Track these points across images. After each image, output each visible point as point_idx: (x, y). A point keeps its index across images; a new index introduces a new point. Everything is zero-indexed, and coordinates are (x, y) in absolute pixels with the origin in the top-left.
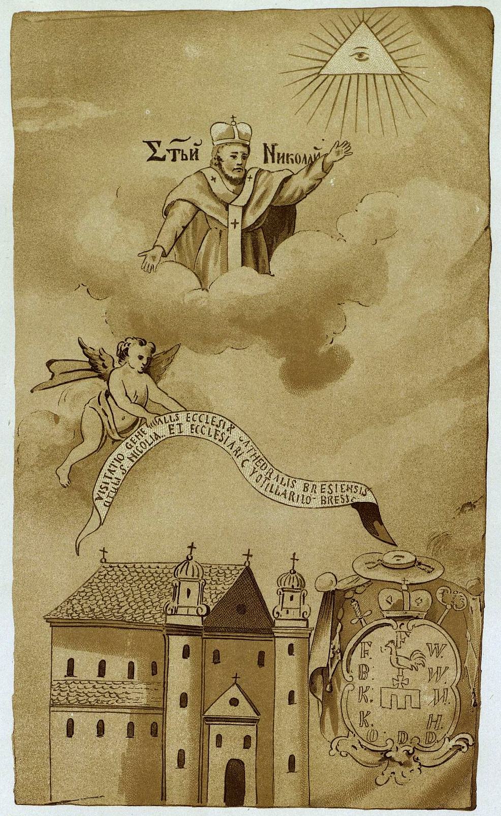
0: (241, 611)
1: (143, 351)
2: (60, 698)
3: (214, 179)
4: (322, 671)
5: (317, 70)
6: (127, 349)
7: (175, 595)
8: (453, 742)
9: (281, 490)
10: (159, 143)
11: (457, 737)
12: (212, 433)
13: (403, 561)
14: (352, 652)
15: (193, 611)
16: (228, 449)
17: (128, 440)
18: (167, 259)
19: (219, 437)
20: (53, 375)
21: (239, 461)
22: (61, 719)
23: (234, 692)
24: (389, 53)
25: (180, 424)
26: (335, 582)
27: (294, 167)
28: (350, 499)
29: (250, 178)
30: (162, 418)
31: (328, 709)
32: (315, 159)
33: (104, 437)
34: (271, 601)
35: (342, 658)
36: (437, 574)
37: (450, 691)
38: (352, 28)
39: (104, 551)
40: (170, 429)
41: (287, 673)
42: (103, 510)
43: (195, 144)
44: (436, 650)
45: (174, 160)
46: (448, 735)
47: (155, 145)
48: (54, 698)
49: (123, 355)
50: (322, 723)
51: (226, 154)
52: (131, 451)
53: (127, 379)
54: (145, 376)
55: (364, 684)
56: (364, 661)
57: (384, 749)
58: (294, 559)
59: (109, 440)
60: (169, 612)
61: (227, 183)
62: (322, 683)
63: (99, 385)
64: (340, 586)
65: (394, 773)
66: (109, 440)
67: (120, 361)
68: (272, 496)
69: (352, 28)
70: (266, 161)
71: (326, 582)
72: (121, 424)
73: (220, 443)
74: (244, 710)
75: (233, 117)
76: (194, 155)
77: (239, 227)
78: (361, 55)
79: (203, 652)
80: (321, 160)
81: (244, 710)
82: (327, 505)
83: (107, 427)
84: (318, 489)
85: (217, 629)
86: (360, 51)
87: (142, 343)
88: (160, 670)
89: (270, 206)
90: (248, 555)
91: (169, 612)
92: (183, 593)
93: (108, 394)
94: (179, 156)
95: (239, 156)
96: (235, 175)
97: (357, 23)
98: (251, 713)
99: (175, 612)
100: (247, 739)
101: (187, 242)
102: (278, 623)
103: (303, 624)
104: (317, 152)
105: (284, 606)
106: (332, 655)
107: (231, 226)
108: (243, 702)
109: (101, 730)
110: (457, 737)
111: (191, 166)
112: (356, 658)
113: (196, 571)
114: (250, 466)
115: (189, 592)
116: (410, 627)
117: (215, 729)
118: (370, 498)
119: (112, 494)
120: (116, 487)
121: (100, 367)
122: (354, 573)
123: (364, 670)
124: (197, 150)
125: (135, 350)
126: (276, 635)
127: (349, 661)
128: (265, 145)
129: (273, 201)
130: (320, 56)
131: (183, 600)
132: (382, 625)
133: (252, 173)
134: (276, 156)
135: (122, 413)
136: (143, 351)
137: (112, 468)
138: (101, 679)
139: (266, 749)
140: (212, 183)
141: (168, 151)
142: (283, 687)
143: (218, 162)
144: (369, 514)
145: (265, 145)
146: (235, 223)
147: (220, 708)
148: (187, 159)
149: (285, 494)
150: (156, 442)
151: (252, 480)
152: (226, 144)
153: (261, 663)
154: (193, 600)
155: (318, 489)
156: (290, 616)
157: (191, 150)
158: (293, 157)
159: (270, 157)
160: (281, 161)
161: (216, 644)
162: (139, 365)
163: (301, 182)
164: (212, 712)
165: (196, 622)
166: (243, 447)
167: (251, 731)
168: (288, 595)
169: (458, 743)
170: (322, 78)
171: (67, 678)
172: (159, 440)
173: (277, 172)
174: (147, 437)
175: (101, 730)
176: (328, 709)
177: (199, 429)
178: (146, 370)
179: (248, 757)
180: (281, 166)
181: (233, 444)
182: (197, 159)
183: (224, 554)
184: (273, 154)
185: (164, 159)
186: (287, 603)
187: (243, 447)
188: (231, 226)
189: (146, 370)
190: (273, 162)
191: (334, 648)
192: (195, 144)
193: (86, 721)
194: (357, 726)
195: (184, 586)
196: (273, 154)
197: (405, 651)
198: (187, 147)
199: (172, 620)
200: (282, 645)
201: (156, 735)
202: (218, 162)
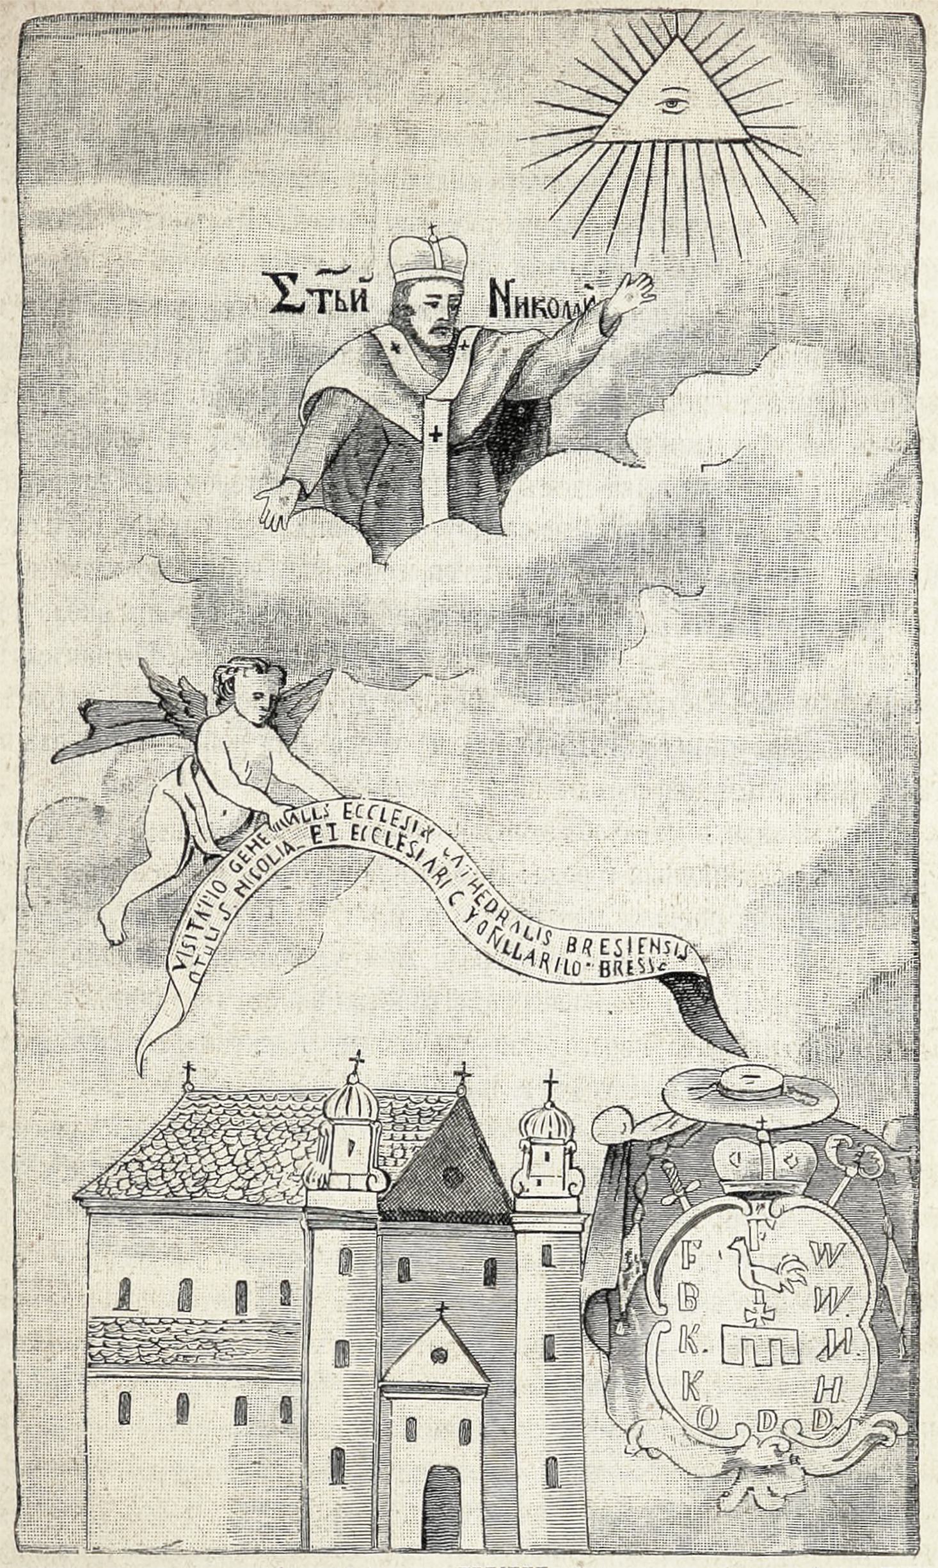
0: (445, 1182)
1: (268, 684)
3: (396, 348)
4: (607, 1295)
5: (587, 135)
6: (232, 680)
7: (326, 1153)
8: (866, 1429)
9: (524, 951)
10: (293, 277)
11: (874, 1419)
12: (394, 841)
13: (757, 1085)
14: (664, 1260)
15: (359, 1182)
16: (423, 872)
17: (234, 856)
18: (309, 502)
19: (406, 849)
20: (93, 728)
21: (444, 894)
23: (440, 1337)
24: (644, 73)
25: (332, 825)
26: (629, 1127)
27: (550, 325)
28: (656, 965)
29: (464, 346)
30: (298, 813)
32: (587, 308)
33: (190, 849)
36: (826, 1106)
37: (857, 1332)
38: (656, 48)
39: (188, 1067)
40: (314, 835)
42: (187, 988)
43: (362, 280)
44: (827, 1255)
45: (322, 310)
46: (857, 1416)
47: (285, 280)
48: (94, 1351)
49: (225, 691)
51: (417, 296)
52: (240, 876)
53: (233, 736)
54: (267, 730)
55: (690, 1319)
56: (687, 1276)
57: (731, 1443)
59: (198, 858)
61: (423, 357)
62: (607, 1314)
63: (174, 750)
64: (644, 1133)
65: (752, 1489)
66: (198, 858)
67: (218, 703)
68: (507, 960)
69: (656, 48)
70: (493, 313)
71: (615, 1131)
72: (224, 826)
73: (410, 861)
74: (459, 1370)
75: (432, 227)
76: (360, 302)
77: (443, 441)
78: (673, 102)
80: (600, 308)
81: (459, 1370)
82: (612, 979)
83: (193, 830)
84: (595, 948)
86: (673, 95)
87: (262, 668)
88: (297, 1292)
89: (503, 399)
90: (462, 1074)
91: (314, 1186)
92: (341, 1147)
93: (197, 767)
94: (330, 300)
95: (444, 302)
96: (433, 341)
97: (665, 40)
99: (324, 1186)
100: (465, 1427)
101: (361, 478)
102: (521, 1205)
103: (572, 1205)
104: (589, 294)
105: (534, 1171)
107: (428, 440)
108: (454, 1350)
109: (183, 1406)
110: (874, 1419)
111: (358, 321)
112: (673, 1272)
114: (464, 904)
116: (776, 1211)
117: (403, 1409)
118: (691, 965)
119: (205, 959)
120: (213, 945)
121: (181, 716)
122: (665, 1109)
123: (690, 1297)
124: (364, 291)
125: (248, 683)
126: (517, 1227)
127: (659, 1276)
128: (493, 281)
129: (508, 390)
130: (597, 105)
132: (723, 1208)
133: (468, 336)
134: (512, 301)
135: (223, 804)
136: (268, 684)
137: (204, 908)
140: (391, 355)
141: (311, 292)
142: (532, 1324)
143: (401, 314)
144: (691, 991)
145: (493, 281)
146: (436, 435)
147: (414, 1366)
148: (345, 310)
149: (532, 956)
150: (288, 858)
151: (470, 929)
152: (420, 280)
153: (490, 1279)
154: (359, 1163)
155: (595, 948)
156: (542, 1191)
157: (353, 293)
158: (544, 305)
159: (500, 305)
160: (522, 311)
161: (398, 1247)
162: (254, 712)
163: (561, 352)
164: (400, 1373)
165: (369, 1202)
166: (451, 867)
167: (471, 1409)
169: (877, 1430)
170: (599, 149)
172: (293, 854)
173: (518, 335)
174: (270, 850)
175: (183, 1406)
177: (368, 834)
178: (270, 720)
180: (521, 322)
181: (433, 861)
182: (364, 309)
183: (403, 1068)
184: (506, 299)
185: (300, 310)
187: (451, 867)
188: (428, 440)
189: (270, 720)
190: (508, 315)
191: (629, 1254)
192: (362, 280)
194: (677, 1402)
195: (342, 1135)
196: (506, 299)
197: (768, 1254)
198: (345, 285)
200: (529, 1247)
202: (401, 314)
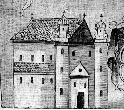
2: (18, 69)
7: (58, 31)
15: (65, 36)
22: (17, 77)
31: (115, 61)
34: (93, 32)
35: (119, 53)
41: (99, 59)
50: (112, 80)
58: (101, 17)
60: (56, 37)
79: (69, 52)
81: (84, 73)
85: (75, 43)
90: (84, 15)
98: (87, 75)
102: (96, 41)
105: (98, 34)
106: (115, 52)
113: (65, 20)
115: (63, 29)
117: (73, 80)
126: (95, 45)
131: (61, 32)
138: (32, 62)
139: (92, 92)
142: (98, 64)
147: (75, 72)
161: (73, 49)
165: (67, 41)
167: (86, 81)
168: (99, 30)
171: (19, 62)
176: (115, 61)
179: (85, 91)
183: (73, 14)
186: (99, 33)
193: (26, 78)
195: (61, 27)
199: (57, 40)
200: (97, 49)
201: (52, 83)
